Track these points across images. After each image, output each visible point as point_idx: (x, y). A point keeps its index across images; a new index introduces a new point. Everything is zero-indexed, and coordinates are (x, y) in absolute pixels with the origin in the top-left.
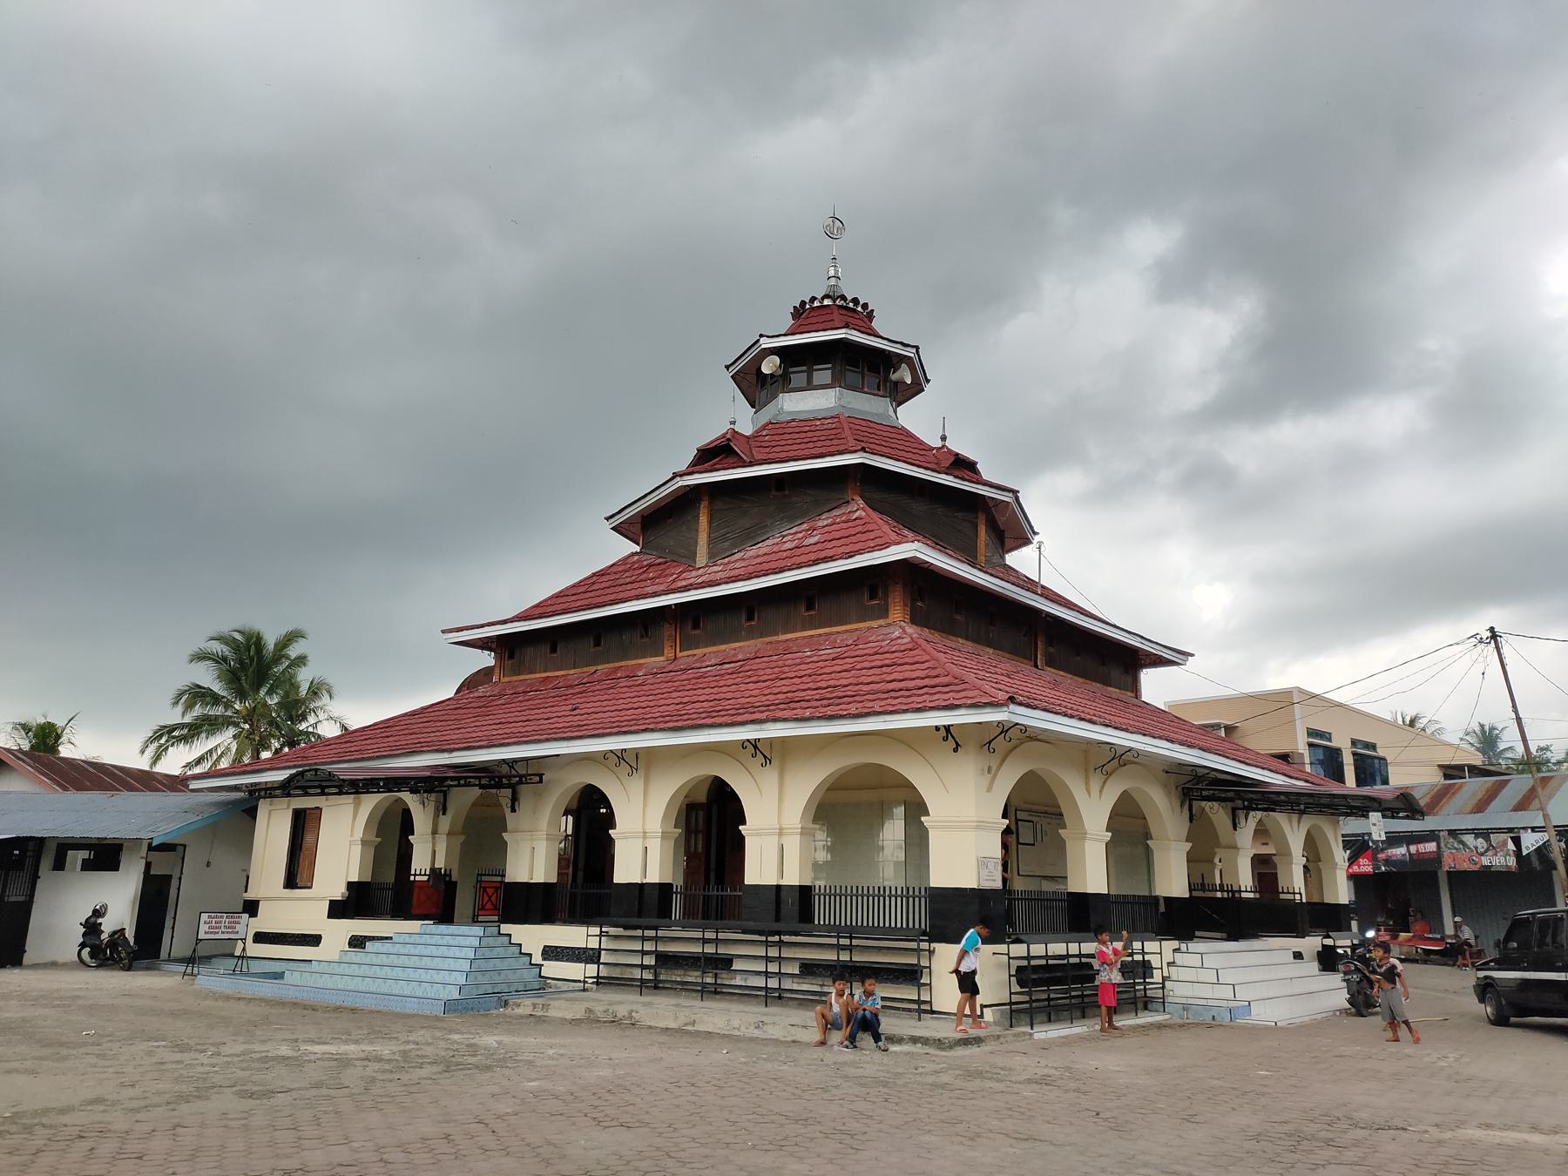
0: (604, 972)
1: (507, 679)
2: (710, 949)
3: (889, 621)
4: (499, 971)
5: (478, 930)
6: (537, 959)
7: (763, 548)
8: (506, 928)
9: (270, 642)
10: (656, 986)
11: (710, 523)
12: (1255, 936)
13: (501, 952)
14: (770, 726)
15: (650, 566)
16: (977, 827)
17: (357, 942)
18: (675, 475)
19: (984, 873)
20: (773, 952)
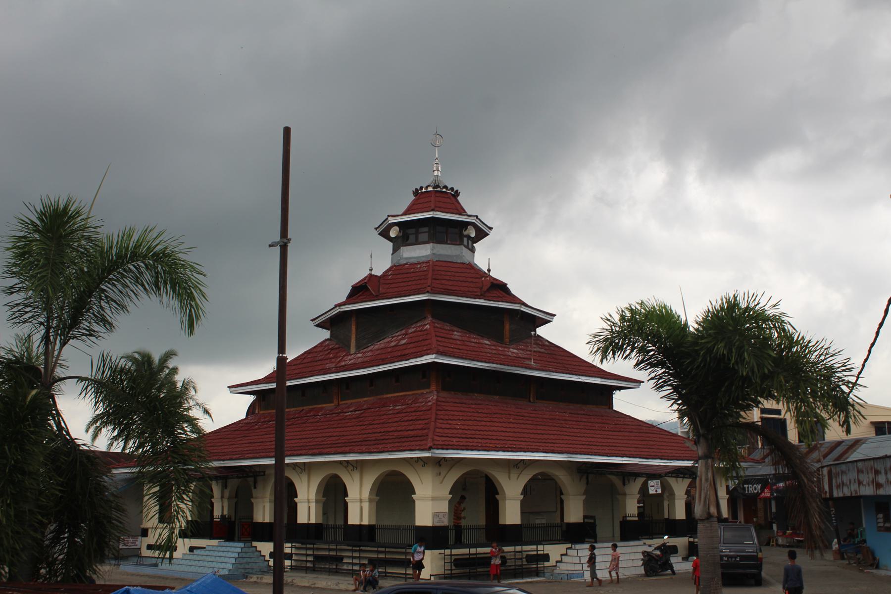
0: (294, 563)
1: (261, 412)
2: (332, 553)
4: (248, 563)
5: (241, 545)
6: (267, 558)
7: (381, 344)
8: (255, 544)
9: (156, 359)
10: (313, 570)
11: (357, 329)
13: (251, 555)
15: (332, 349)
16: (432, 500)
17: (192, 549)
18: (336, 306)
19: (437, 520)
20: (356, 554)
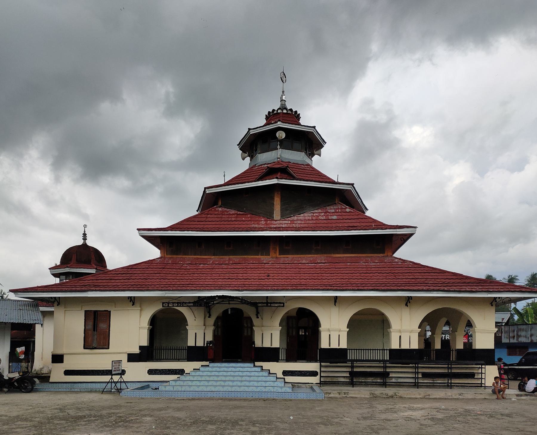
3: (385, 255)
12: (237, 362)
14: (89, 293)
